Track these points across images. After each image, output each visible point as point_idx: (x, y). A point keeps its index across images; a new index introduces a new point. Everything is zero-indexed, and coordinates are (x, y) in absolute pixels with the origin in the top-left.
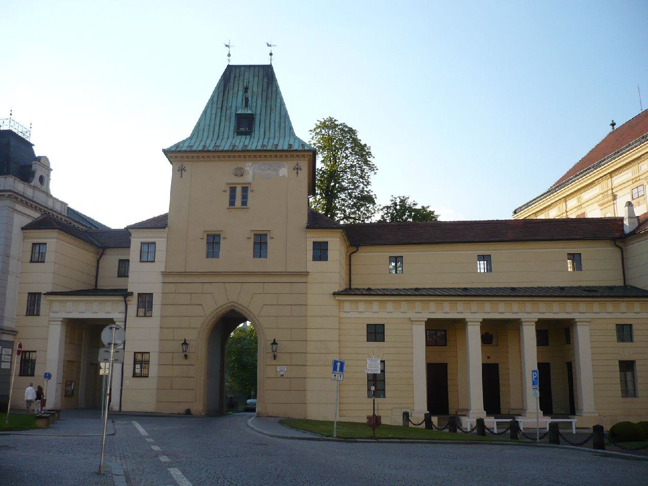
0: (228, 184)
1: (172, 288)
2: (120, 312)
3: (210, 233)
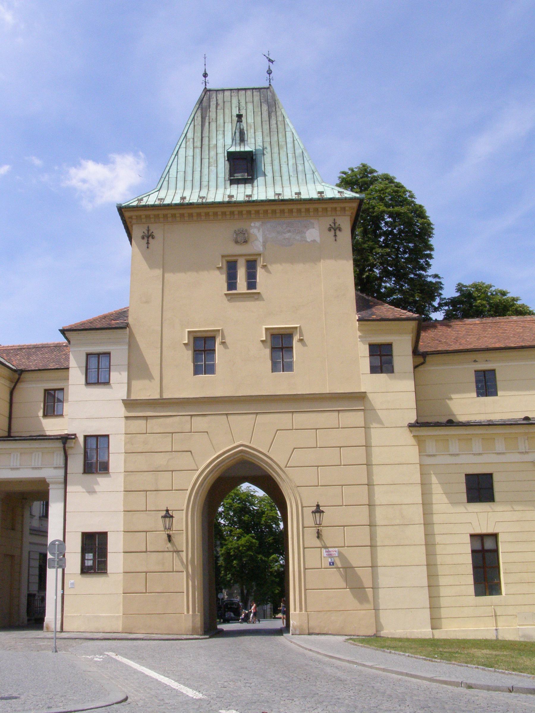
0: (223, 256)
1: (139, 425)
2: (55, 468)
3: (199, 335)
